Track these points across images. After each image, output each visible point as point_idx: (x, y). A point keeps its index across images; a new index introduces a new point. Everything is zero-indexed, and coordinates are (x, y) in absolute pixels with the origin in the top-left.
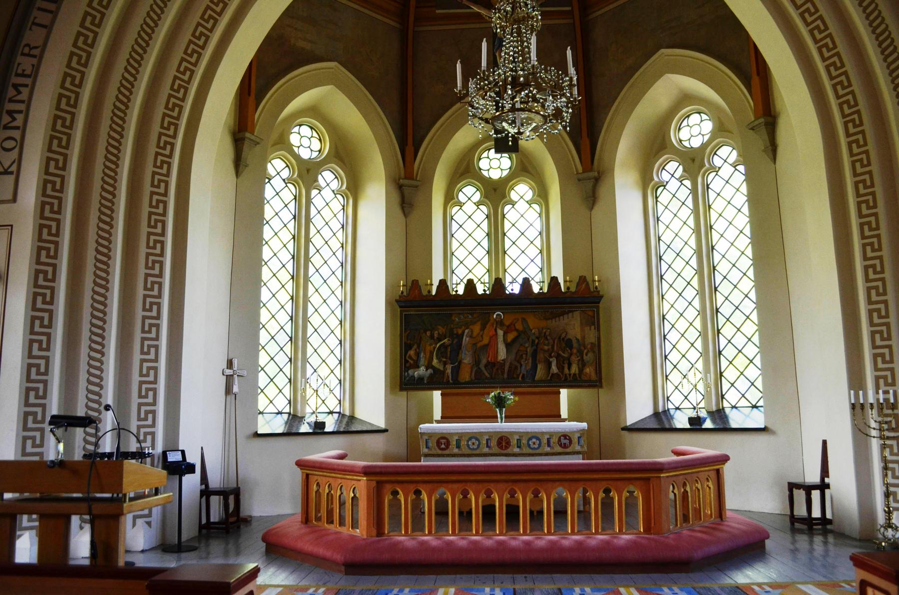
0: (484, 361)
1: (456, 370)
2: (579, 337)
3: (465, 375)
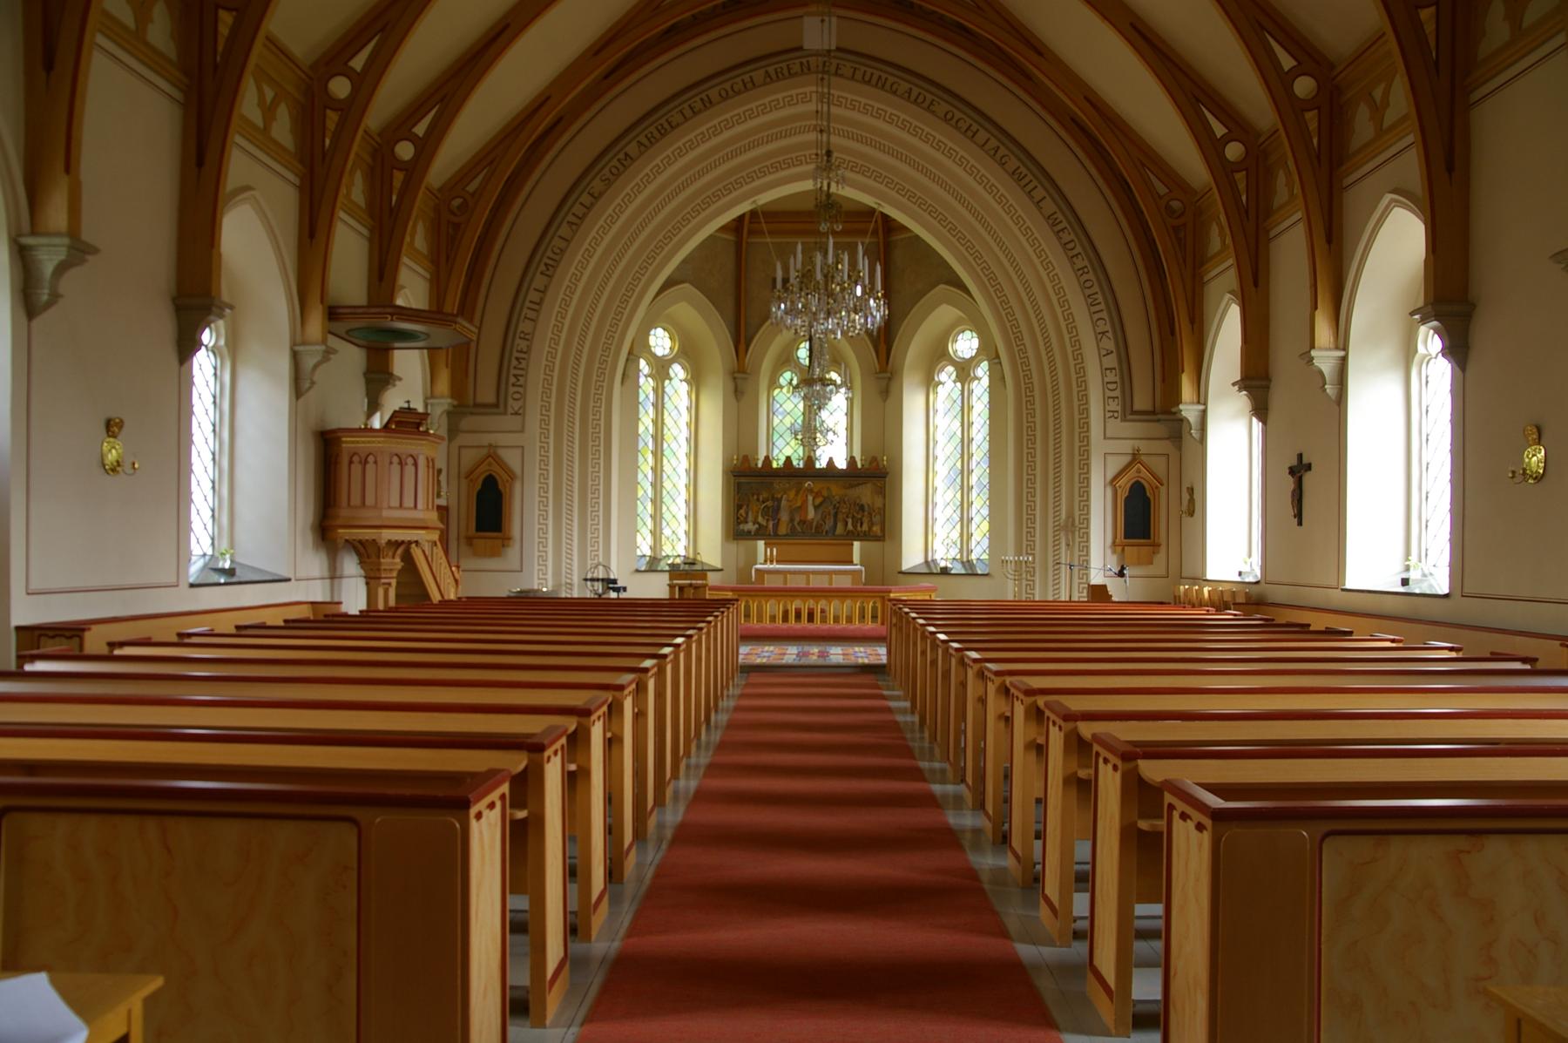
0: (797, 519)
1: (776, 526)
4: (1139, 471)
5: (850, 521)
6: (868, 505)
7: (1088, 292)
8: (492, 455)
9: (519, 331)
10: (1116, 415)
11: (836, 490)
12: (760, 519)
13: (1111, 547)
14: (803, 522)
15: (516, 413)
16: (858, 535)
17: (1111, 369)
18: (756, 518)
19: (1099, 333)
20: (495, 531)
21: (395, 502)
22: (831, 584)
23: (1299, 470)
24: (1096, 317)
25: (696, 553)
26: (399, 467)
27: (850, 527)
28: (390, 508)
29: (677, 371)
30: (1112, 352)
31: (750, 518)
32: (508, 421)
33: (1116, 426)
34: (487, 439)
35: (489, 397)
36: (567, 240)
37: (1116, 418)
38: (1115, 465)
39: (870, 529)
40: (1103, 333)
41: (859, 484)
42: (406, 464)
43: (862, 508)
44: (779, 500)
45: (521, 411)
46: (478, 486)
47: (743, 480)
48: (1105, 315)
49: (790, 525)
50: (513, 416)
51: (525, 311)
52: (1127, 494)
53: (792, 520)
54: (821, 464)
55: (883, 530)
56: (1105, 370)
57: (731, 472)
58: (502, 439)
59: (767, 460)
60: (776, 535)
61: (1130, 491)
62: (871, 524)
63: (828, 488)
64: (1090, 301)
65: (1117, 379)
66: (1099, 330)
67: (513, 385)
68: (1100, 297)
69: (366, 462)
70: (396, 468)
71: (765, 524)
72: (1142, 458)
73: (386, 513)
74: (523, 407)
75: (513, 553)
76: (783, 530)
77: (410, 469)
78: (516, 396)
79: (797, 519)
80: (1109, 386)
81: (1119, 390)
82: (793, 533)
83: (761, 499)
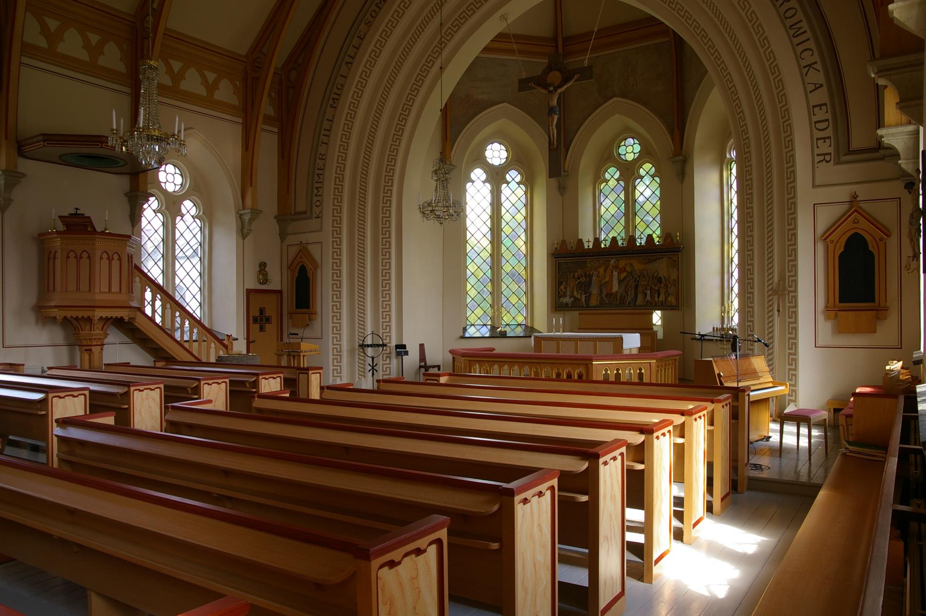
0: (604, 293)
1: (588, 299)
2: (666, 276)
3: (594, 302)
4: (856, 222)
5: (648, 292)
6: (665, 278)
7: (789, 22)
8: (303, 250)
9: (318, 154)
10: (828, 158)
11: (637, 266)
12: (575, 293)
13: (823, 312)
14: (609, 295)
15: (318, 217)
16: (656, 305)
17: (820, 106)
18: (573, 292)
19: (804, 67)
22: (576, 351)
24: (800, 49)
25: (212, 326)
26: (107, 261)
27: (648, 298)
28: (101, 292)
29: (514, 176)
30: (821, 86)
31: (568, 293)
33: (829, 171)
35: (301, 207)
36: (345, 77)
37: (827, 162)
38: (826, 217)
39: (666, 299)
40: (810, 66)
41: (655, 260)
42: (113, 259)
43: (660, 280)
44: (591, 276)
47: (562, 260)
48: (811, 44)
49: (599, 298)
50: (316, 219)
51: (322, 137)
52: (842, 250)
53: (601, 292)
54: (641, 241)
55: (677, 299)
56: (812, 109)
57: (552, 254)
59: (597, 241)
60: (588, 306)
61: (610, 243)
62: (667, 294)
63: (631, 264)
64: (792, 32)
65: (829, 116)
66: (804, 63)
67: (316, 196)
68: (805, 26)
70: (105, 262)
71: (579, 297)
72: (863, 205)
73: (98, 297)
74: (321, 212)
75: (317, 323)
76: (594, 302)
77: (115, 263)
78: (318, 203)
79: (604, 293)
80: (819, 126)
81: (830, 128)
82: (602, 305)
83: (576, 276)
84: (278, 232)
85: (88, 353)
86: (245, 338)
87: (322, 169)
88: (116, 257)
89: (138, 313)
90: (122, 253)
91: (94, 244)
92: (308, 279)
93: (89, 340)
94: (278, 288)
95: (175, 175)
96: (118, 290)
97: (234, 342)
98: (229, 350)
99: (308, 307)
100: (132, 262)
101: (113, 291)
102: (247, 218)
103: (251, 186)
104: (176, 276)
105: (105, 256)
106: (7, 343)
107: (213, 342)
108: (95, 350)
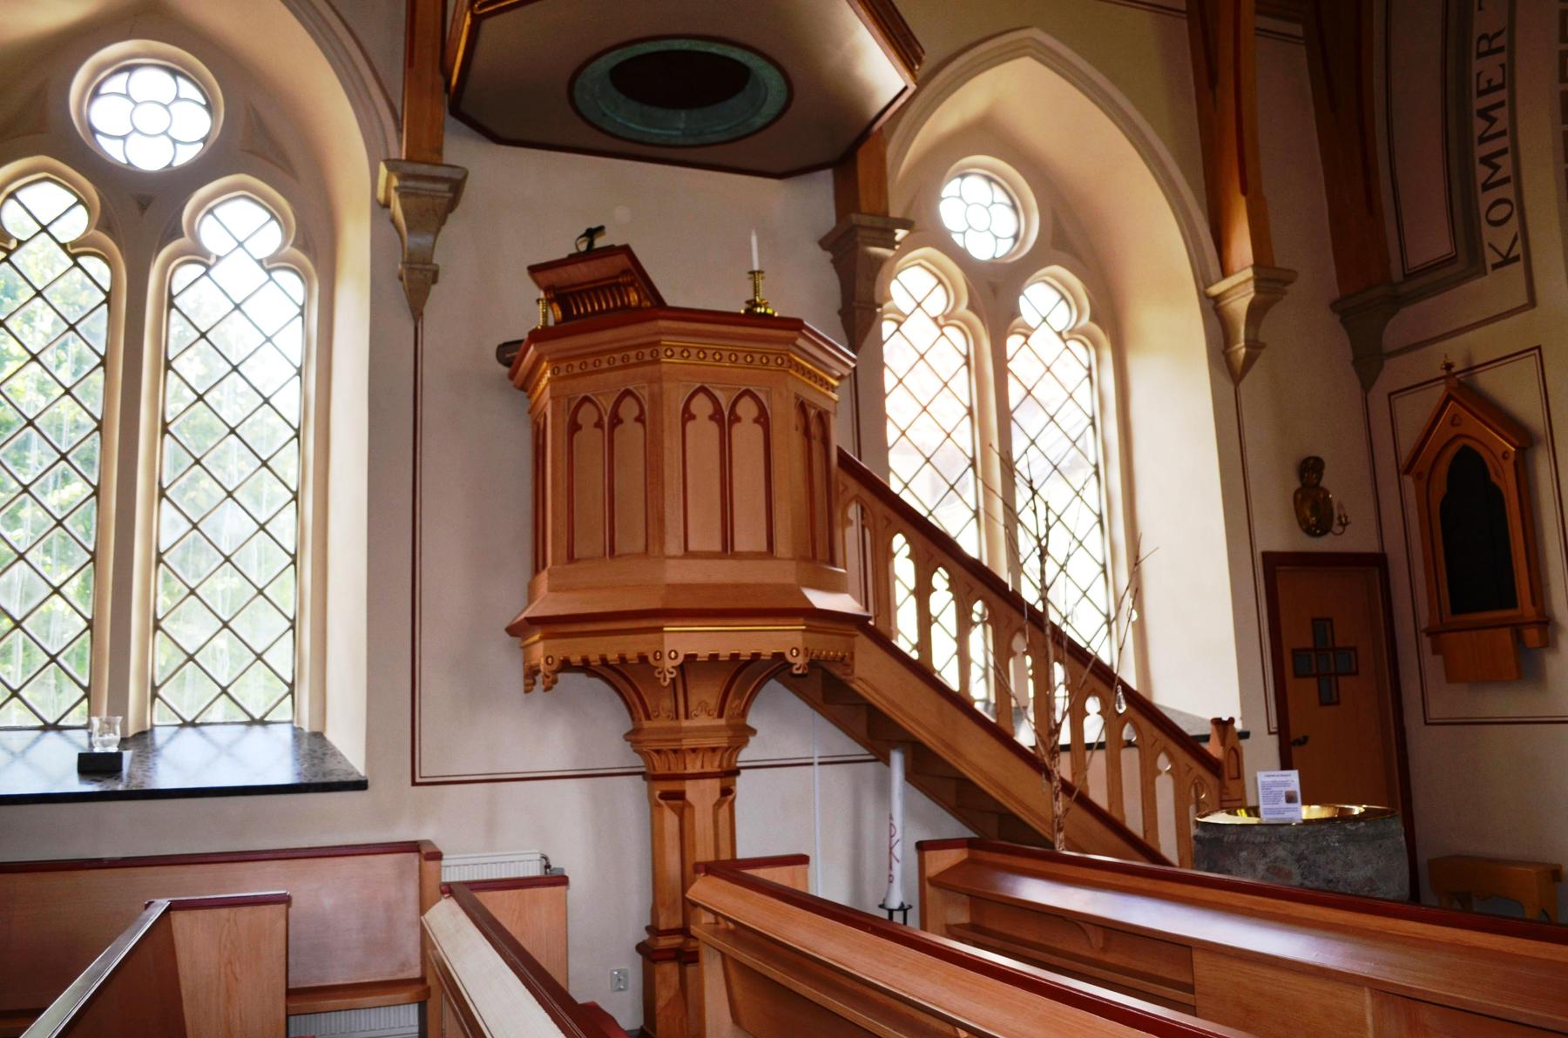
15: (1507, 260)
20: (1501, 607)
21: (706, 537)
23: (1136, 564)
26: (713, 428)
28: (688, 553)
32: (1502, 287)
34: (1430, 363)
45: (1518, 249)
46: (1440, 487)
58: (1482, 343)
69: (616, 420)
70: (704, 434)
77: (747, 436)
78: (1499, 213)
84: (1352, 359)
85: (672, 808)
86: (1274, 724)
87: (1501, 87)
88: (747, 409)
89: (862, 643)
90: (768, 394)
91: (656, 361)
92: (1495, 497)
93: (672, 756)
94: (1369, 545)
95: (993, 209)
96: (763, 547)
97: (1243, 743)
98: (1228, 783)
99: (1508, 599)
100: (826, 441)
101: (738, 548)
102: (1240, 305)
103: (1244, 192)
104: (1019, 525)
105: (702, 406)
106: (428, 770)
107: (1165, 750)
108: (701, 794)
